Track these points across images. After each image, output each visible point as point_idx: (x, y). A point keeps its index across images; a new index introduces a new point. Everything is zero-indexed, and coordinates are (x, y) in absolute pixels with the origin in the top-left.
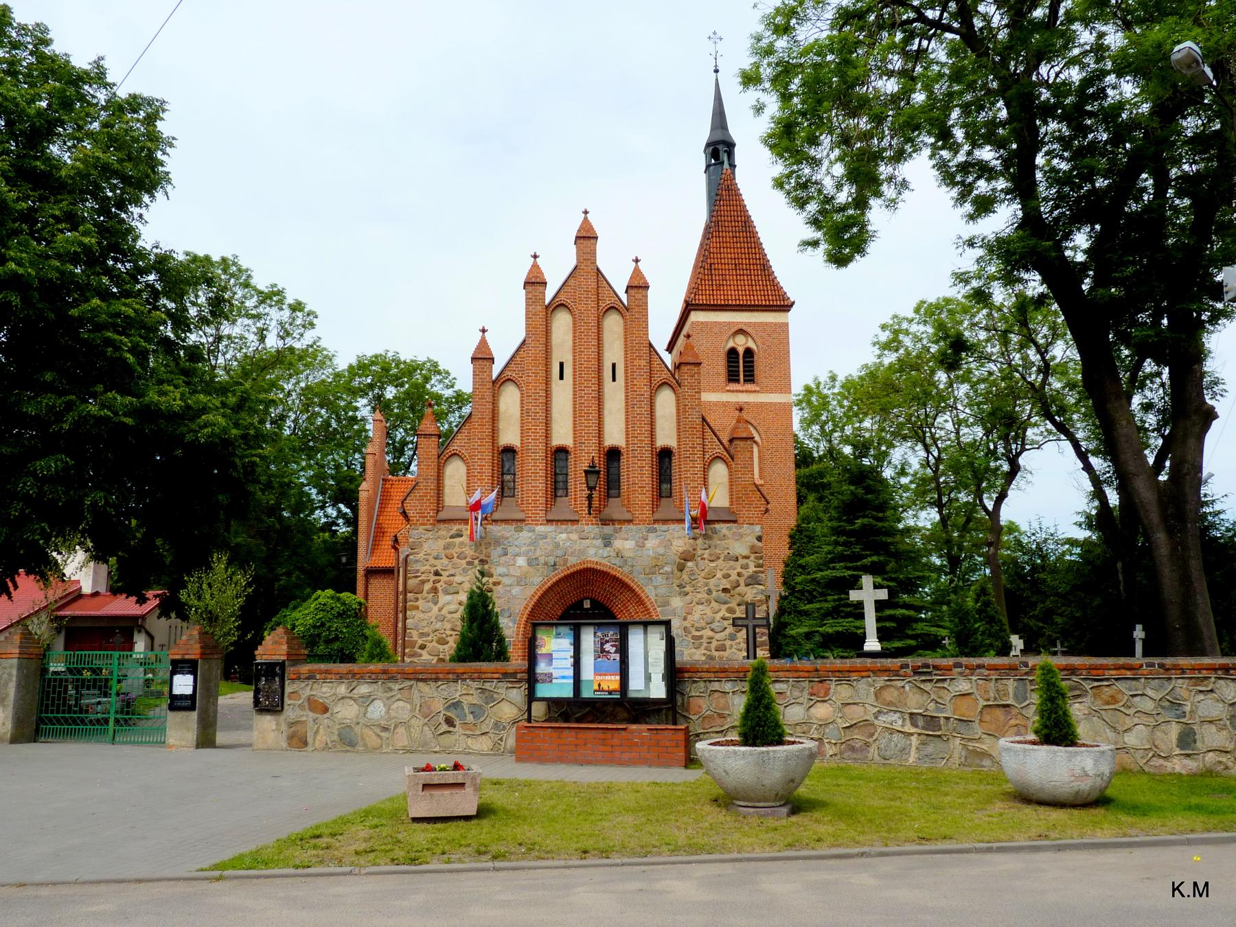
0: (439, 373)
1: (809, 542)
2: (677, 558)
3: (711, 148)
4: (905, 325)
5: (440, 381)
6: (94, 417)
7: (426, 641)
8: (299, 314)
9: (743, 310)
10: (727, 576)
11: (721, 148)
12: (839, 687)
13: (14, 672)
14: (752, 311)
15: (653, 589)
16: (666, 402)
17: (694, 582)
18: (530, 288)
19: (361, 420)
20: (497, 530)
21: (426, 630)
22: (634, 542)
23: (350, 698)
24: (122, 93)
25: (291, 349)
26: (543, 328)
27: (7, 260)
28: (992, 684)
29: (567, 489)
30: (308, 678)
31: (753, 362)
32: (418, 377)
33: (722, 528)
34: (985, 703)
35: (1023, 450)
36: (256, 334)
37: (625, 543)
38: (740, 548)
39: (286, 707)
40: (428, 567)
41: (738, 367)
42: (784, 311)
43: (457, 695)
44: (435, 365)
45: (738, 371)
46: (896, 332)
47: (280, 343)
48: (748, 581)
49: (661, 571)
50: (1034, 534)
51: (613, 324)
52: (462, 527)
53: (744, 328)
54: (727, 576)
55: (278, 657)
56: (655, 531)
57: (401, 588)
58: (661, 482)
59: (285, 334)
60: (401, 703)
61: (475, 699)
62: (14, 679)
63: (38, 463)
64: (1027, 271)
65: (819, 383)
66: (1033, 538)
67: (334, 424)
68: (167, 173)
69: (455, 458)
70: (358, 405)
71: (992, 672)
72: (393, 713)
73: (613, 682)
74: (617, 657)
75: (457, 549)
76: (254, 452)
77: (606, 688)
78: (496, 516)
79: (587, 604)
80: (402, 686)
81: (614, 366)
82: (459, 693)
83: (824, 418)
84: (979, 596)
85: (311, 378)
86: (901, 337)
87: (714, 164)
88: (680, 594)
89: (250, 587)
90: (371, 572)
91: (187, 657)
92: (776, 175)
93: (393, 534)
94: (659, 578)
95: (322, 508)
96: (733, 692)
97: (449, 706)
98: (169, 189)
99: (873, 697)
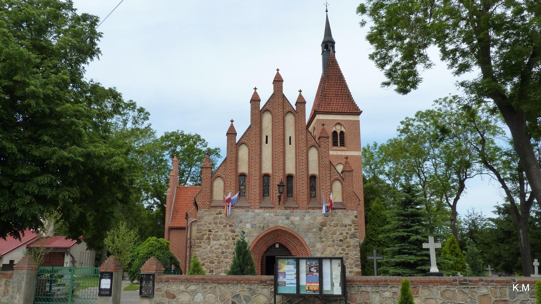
0: (200, 140)
1: (378, 218)
2: (319, 226)
3: (325, 44)
4: (411, 122)
5: (201, 144)
6: (66, 157)
7: (204, 262)
8: (142, 113)
9: (332, 114)
10: (341, 234)
11: (329, 44)
12: (423, 290)
13: (25, 276)
14: (343, 115)
15: (308, 239)
16: (313, 154)
17: (326, 237)
18: (253, 103)
19: (165, 161)
20: (238, 211)
21: (204, 257)
22: (299, 217)
23: (186, 292)
24: (79, 13)
25: (138, 129)
26: (259, 120)
27: (30, 85)
28: (498, 290)
29: (269, 193)
30: (166, 282)
31: (344, 137)
32: (191, 142)
33: (339, 212)
34: (495, 299)
35: (466, 178)
36: (122, 122)
37: (296, 219)
38: (347, 221)
39: (155, 295)
40: (206, 228)
41: (337, 139)
42: (358, 115)
43: (238, 291)
44: (199, 137)
45: (337, 141)
46: (407, 125)
47: (133, 127)
48: (351, 236)
49: (312, 231)
50: (470, 216)
51: (290, 119)
52: (222, 210)
53: (340, 122)
54: (341, 234)
55: (151, 271)
56: (309, 212)
57: (189, 237)
58: (311, 190)
59: (135, 122)
60: (211, 295)
61: (247, 293)
62: (25, 280)
63: (39, 178)
64: (488, 97)
65: (369, 147)
66: (470, 217)
67: (153, 162)
68: (98, 48)
69: (219, 178)
70: (164, 154)
71: (498, 284)
72: (206, 299)
73: (315, 286)
74: (318, 274)
75: (219, 220)
76: (133, 174)
77: (312, 289)
78: (236, 205)
79: (277, 246)
80: (211, 286)
81: (290, 138)
82: (238, 290)
83: (371, 163)
84: (451, 244)
85: (144, 142)
86: (410, 127)
87: (326, 51)
88: (320, 242)
89: (136, 237)
90: (171, 229)
91: (108, 271)
92: (371, 53)
93: (186, 212)
94: (311, 234)
95: (147, 199)
96: (372, 292)
97: (234, 297)
98: (100, 55)
99: (440, 295)
